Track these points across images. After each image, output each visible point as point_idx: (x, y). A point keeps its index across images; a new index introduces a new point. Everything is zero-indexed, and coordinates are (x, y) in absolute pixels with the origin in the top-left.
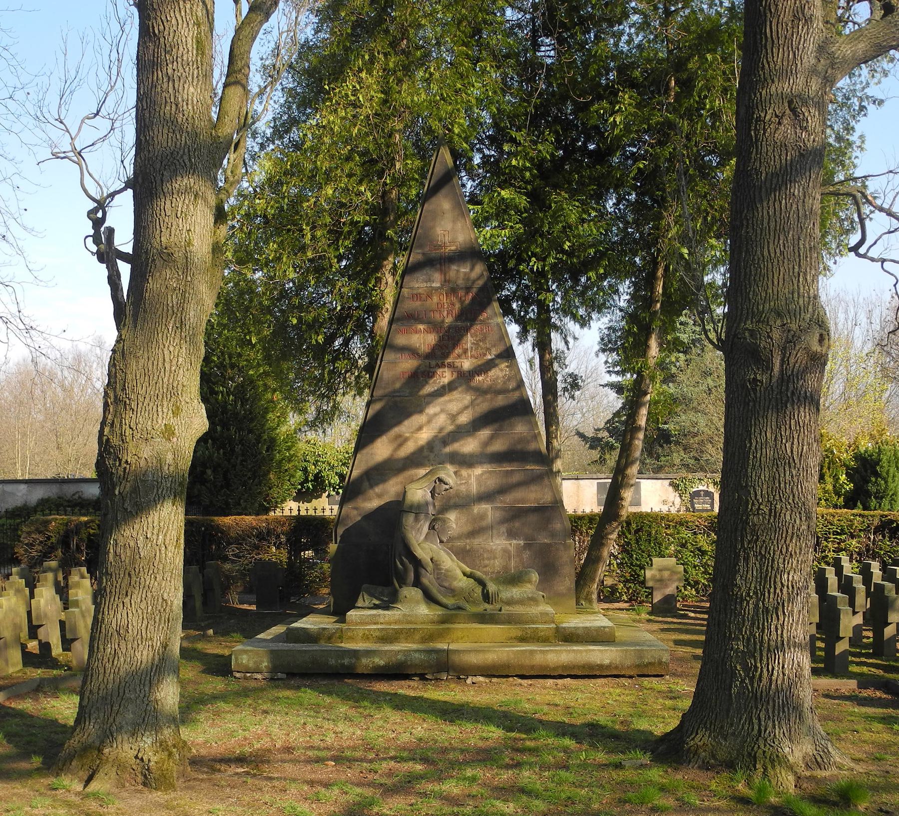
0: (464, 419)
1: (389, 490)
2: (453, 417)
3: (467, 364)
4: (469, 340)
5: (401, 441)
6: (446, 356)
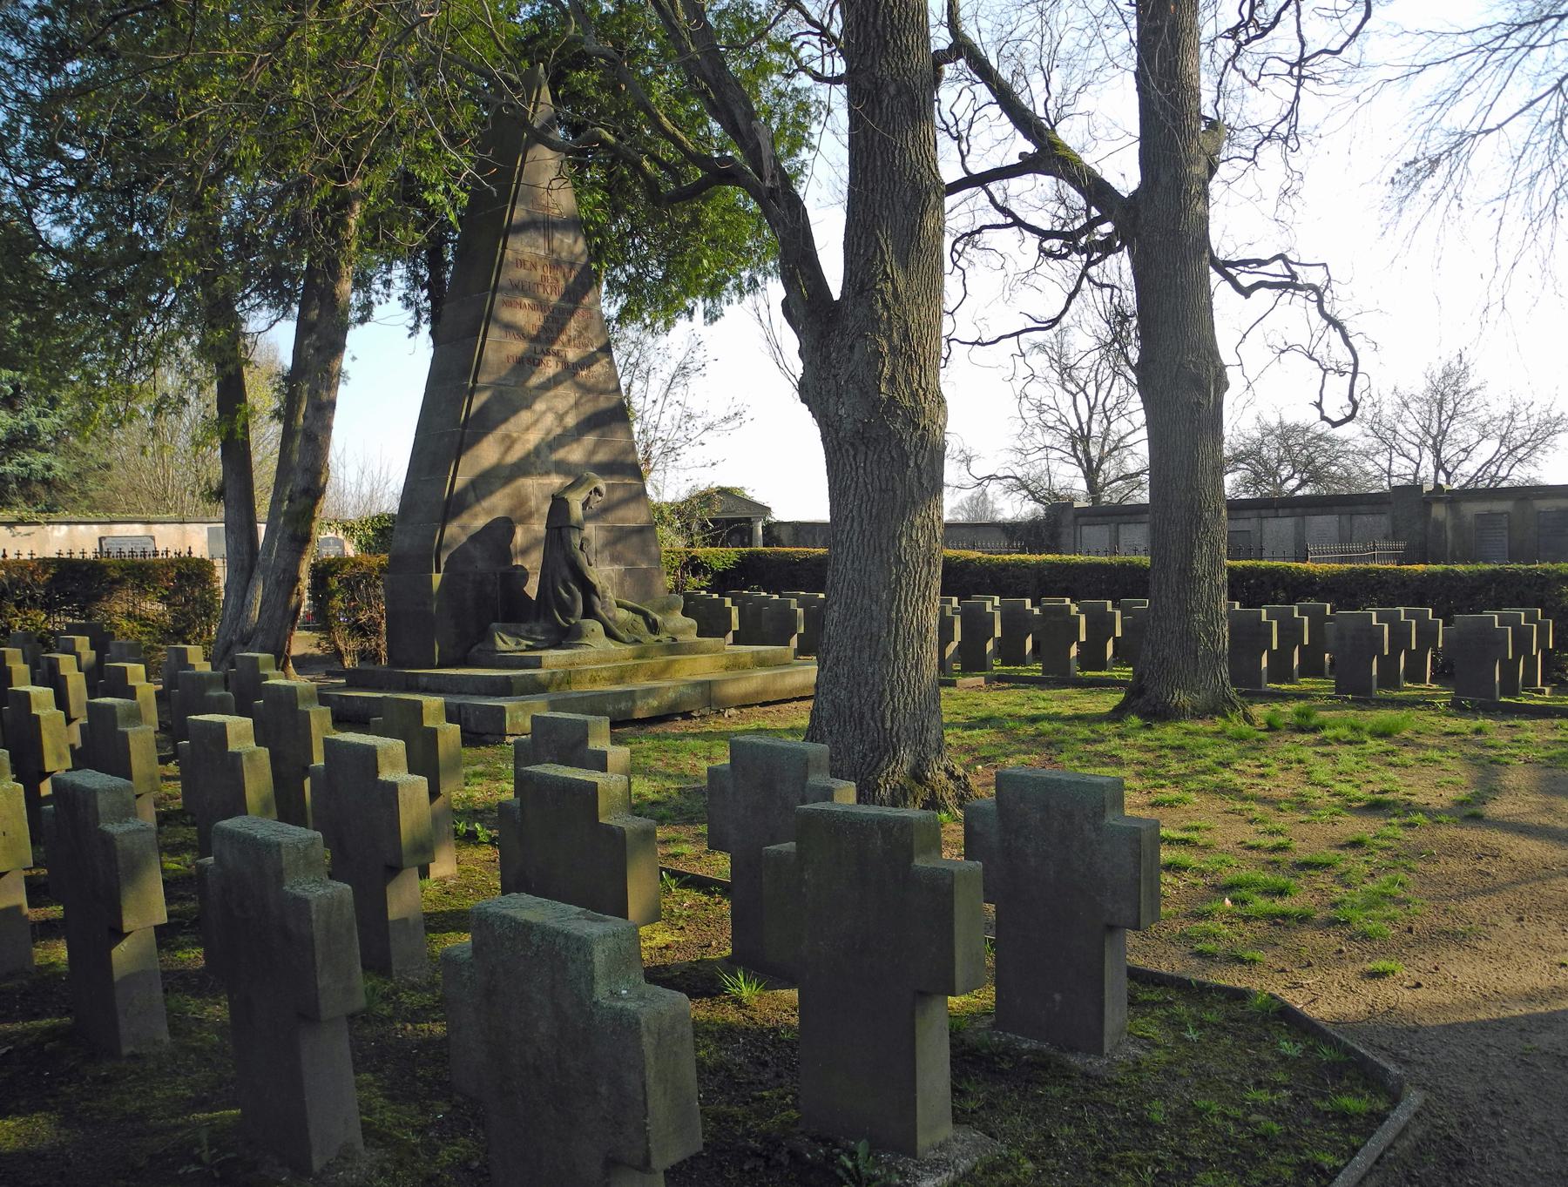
0: (571, 421)
1: (498, 503)
2: (560, 418)
3: (572, 355)
4: (573, 326)
5: (509, 442)
6: (552, 341)
